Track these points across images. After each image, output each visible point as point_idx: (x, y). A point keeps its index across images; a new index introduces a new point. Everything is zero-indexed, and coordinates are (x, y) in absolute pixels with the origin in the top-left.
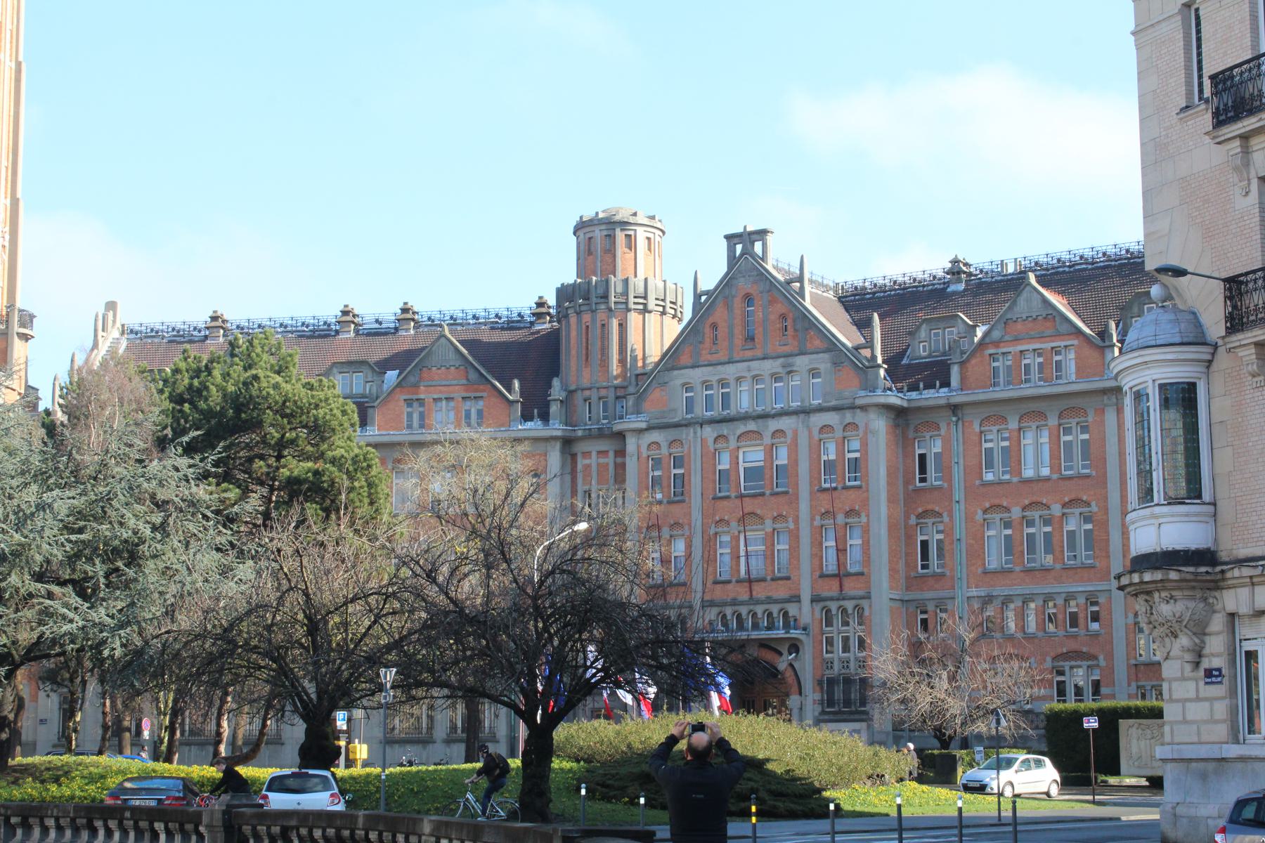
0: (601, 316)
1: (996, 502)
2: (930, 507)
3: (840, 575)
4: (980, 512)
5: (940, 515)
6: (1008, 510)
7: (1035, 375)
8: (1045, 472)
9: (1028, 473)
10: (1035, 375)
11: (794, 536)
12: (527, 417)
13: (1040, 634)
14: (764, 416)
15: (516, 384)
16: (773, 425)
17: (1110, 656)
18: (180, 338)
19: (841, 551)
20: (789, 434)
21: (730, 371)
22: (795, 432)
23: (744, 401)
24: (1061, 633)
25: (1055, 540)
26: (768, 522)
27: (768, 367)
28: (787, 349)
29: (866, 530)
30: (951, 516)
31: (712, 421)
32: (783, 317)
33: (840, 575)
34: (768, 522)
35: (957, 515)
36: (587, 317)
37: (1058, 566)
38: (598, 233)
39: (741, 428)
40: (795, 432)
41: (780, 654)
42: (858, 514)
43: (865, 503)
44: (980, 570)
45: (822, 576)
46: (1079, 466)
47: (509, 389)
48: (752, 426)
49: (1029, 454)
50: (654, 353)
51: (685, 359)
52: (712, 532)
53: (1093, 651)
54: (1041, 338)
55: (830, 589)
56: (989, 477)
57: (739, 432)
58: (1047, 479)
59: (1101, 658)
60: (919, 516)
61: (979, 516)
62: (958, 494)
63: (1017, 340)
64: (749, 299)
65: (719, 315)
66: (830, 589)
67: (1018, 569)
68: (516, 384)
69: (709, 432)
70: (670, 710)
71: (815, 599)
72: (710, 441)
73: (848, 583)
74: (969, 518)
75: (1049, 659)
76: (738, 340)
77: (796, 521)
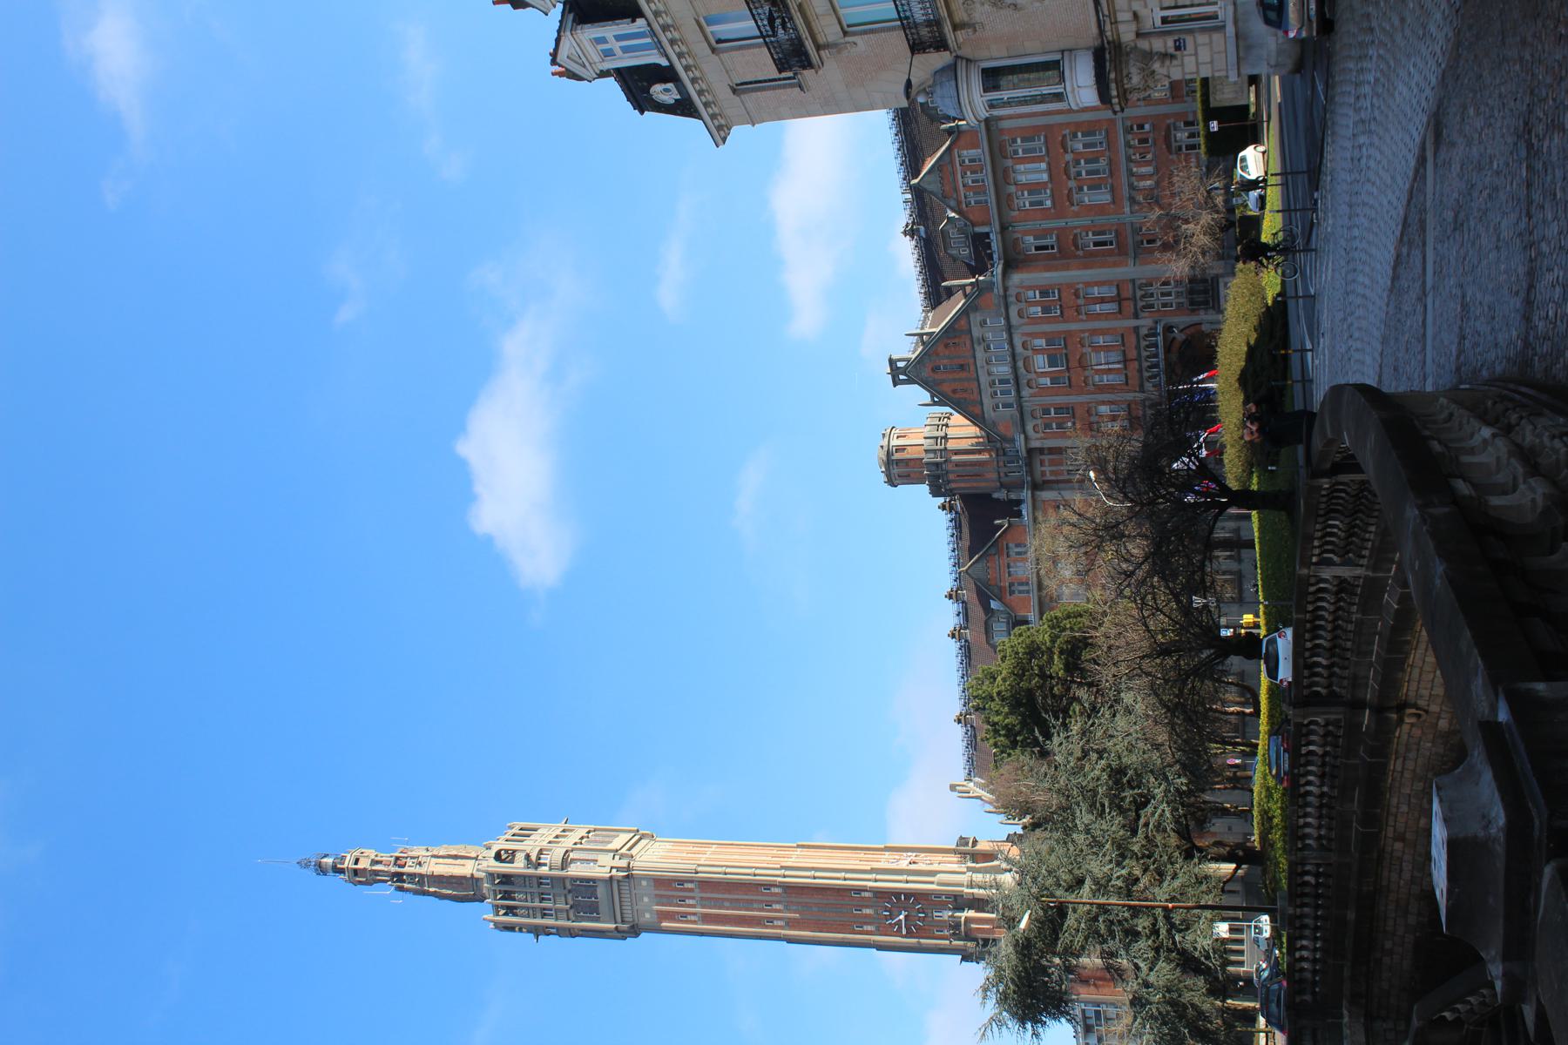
0: (950, 467)
3: (1119, 299)
8: (1043, 166)
9: (1045, 177)
14: (1014, 356)
16: (1019, 349)
18: (973, 743)
19: (1102, 300)
21: (984, 380)
23: (1004, 370)
27: (980, 354)
28: (968, 343)
31: (1018, 391)
32: (946, 346)
33: (1119, 299)
36: (951, 476)
38: (895, 471)
39: (1022, 370)
45: (1120, 312)
46: (1039, 143)
48: (1020, 364)
49: (1033, 178)
50: (973, 430)
51: (977, 410)
54: (954, 173)
55: (1129, 307)
56: (1049, 203)
58: (1049, 164)
61: (1075, 208)
63: (956, 190)
64: (935, 369)
65: (947, 388)
66: (1129, 307)
69: (1026, 392)
71: (1136, 316)
74: (1077, 215)
76: (963, 375)
77: (1083, 331)
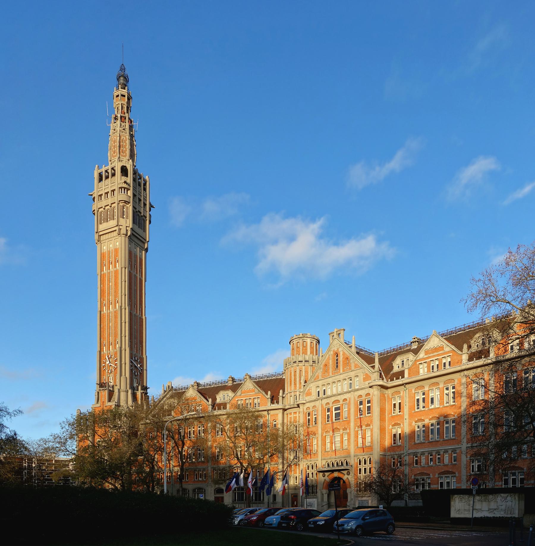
1: (420, 418)
2: (396, 422)
4: (414, 422)
5: (400, 424)
6: (424, 420)
7: (435, 369)
10: (435, 369)
11: (349, 434)
12: (272, 402)
13: (434, 465)
15: (269, 393)
17: (460, 472)
20: (348, 400)
22: (350, 399)
24: (442, 464)
25: (441, 430)
26: (341, 430)
29: (372, 431)
30: (403, 425)
34: (341, 430)
35: (405, 424)
37: (441, 440)
40: (350, 399)
41: (344, 474)
42: (369, 425)
43: (371, 421)
44: (413, 443)
47: (267, 394)
52: (324, 435)
53: (454, 471)
57: (333, 401)
59: (457, 473)
60: (393, 426)
62: (406, 416)
67: (427, 442)
68: (269, 393)
70: (397, 379)
72: (324, 405)
75: (437, 474)
77: (350, 429)
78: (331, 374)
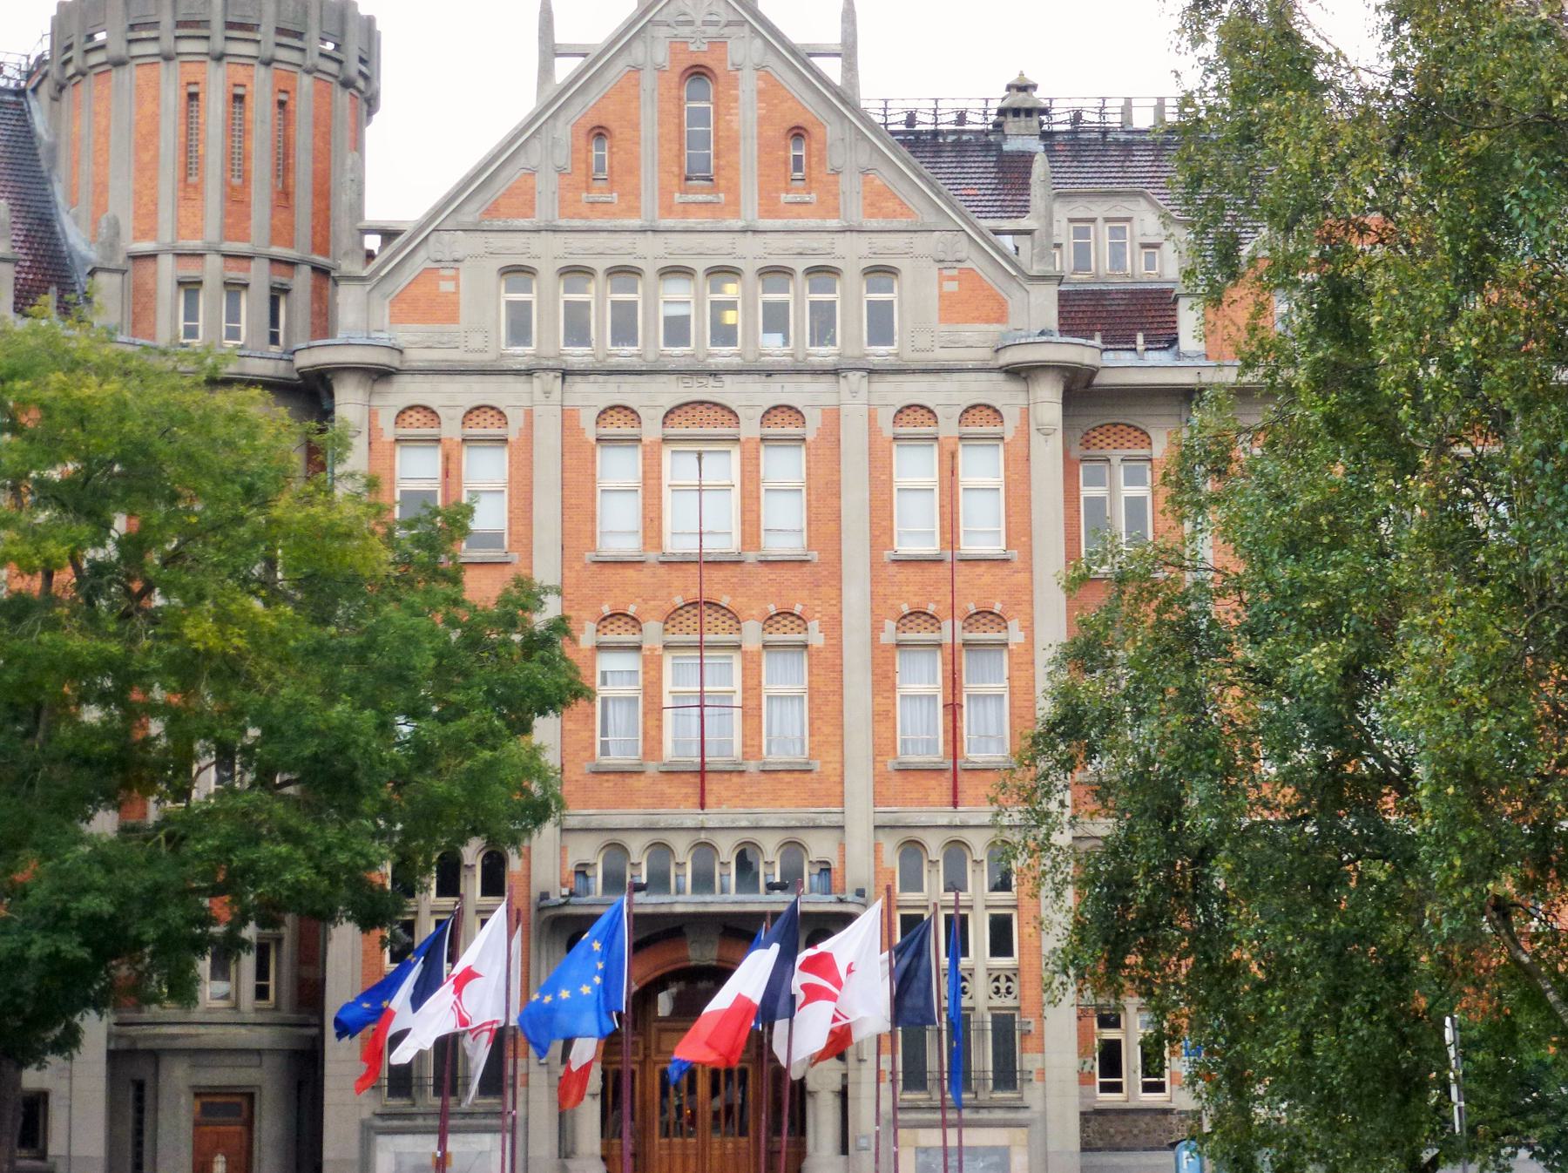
73: (974, 754)
77: (834, 625)
78: (649, 178)
